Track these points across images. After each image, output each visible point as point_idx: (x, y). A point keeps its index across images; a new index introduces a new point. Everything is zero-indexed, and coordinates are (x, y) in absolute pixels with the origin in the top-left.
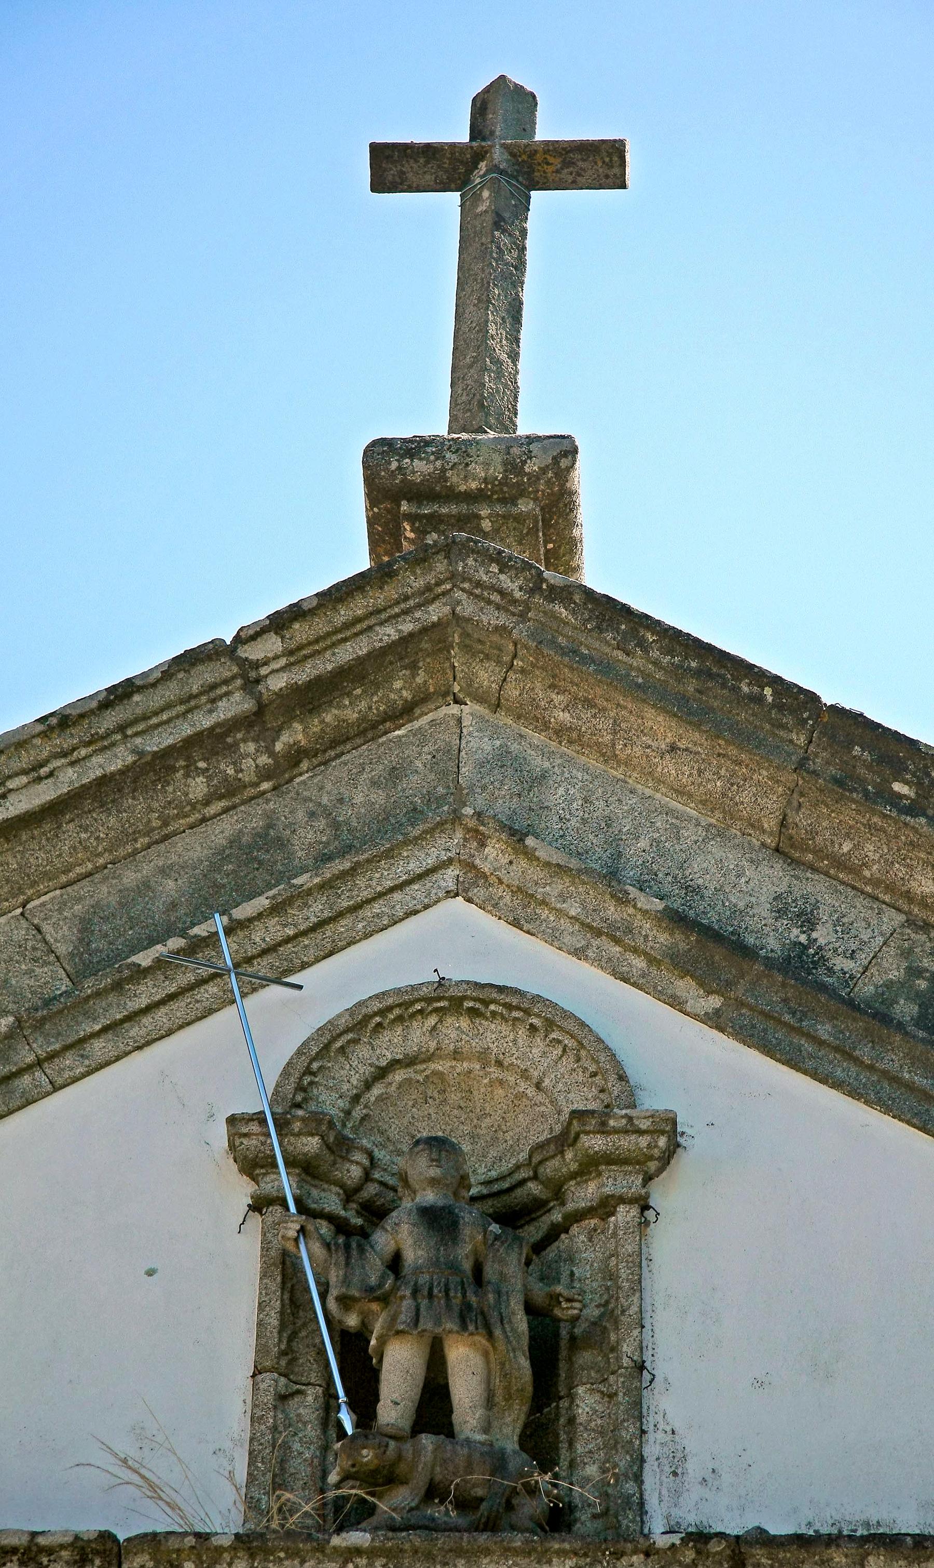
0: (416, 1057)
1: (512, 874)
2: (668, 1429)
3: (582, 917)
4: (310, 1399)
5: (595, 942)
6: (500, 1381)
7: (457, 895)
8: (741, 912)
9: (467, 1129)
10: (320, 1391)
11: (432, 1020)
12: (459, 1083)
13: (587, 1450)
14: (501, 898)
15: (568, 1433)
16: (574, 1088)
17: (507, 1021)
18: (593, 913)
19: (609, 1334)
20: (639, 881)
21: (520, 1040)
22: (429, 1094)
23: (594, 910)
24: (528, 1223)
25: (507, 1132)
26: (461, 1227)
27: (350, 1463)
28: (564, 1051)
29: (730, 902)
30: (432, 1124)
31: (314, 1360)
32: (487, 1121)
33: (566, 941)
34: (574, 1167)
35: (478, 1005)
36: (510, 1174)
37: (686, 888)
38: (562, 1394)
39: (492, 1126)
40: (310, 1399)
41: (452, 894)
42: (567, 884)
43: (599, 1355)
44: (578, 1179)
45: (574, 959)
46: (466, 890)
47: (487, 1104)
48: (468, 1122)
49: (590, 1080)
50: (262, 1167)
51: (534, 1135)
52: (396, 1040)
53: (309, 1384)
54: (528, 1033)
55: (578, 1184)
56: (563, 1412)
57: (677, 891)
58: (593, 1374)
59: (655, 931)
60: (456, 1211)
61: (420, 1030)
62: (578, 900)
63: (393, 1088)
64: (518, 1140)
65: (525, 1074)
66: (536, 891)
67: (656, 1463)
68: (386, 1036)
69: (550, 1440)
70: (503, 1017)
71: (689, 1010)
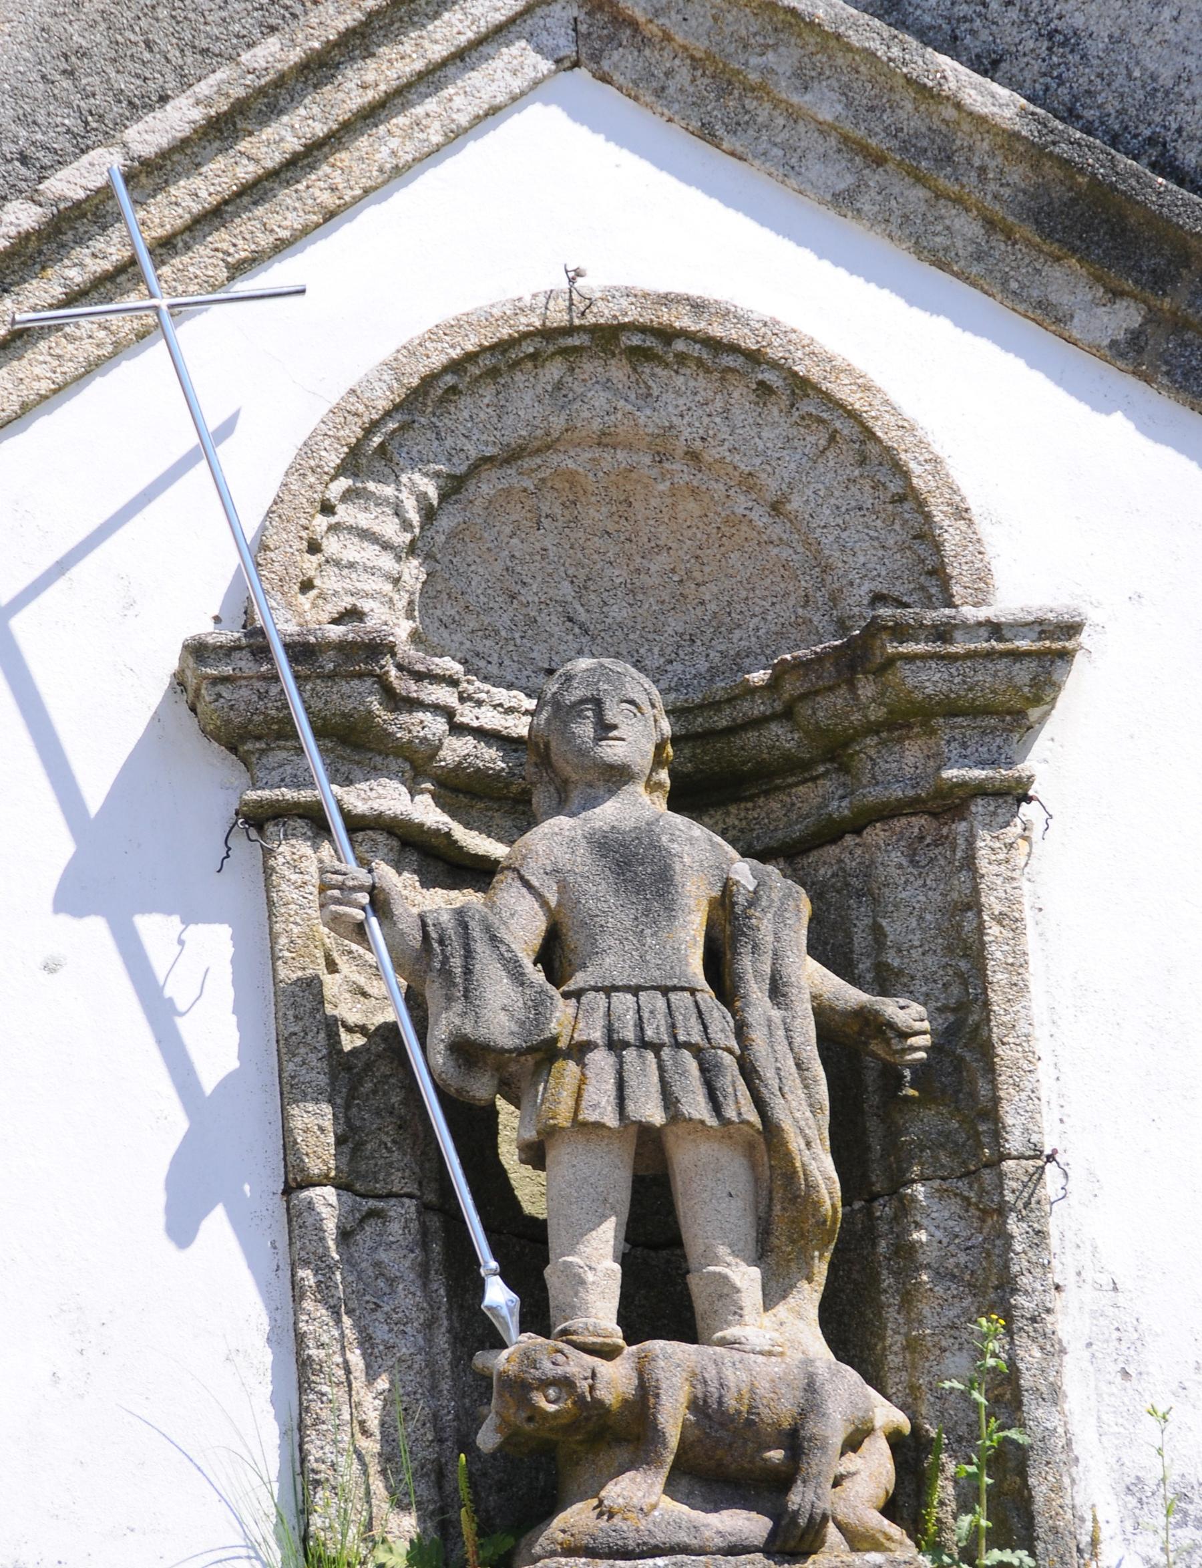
0: (522, 448)
1: (693, 23)
2: (1105, 1280)
3: (848, 127)
4: (395, 1227)
5: (875, 178)
6: (784, 1209)
7: (576, 64)
8: (1167, 93)
9: (619, 574)
10: (413, 1209)
11: (554, 370)
12: (606, 488)
13: (944, 1321)
14: (668, 74)
15: (896, 1274)
16: (855, 519)
17: (708, 371)
18: (870, 115)
19: (973, 1082)
20: (949, 19)
21: (736, 411)
22: (545, 509)
23: (871, 109)
24: (766, 793)
25: (704, 583)
26: (678, 879)
27: (524, 1415)
28: (832, 438)
29: (1144, 69)
30: (550, 569)
31: (394, 1142)
32: (660, 562)
33: (812, 175)
34: (876, 713)
35: (650, 342)
36: (729, 701)
37: (1050, 36)
38: (877, 1188)
39: (673, 571)
40: (395, 1227)
41: (567, 64)
42: (811, 48)
43: (953, 1117)
44: (884, 735)
45: (832, 213)
46: (596, 57)
47: (662, 528)
48: (623, 560)
49: (890, 507)
50: (258, 738)
51: (764, 598)
52: (482, 416)
53: (390, 1195)
54: (753, 397)
55: (883, 743)
56: (883, 1228)
57: (1031, 44)
58: (944, 1159)
59: (1000, 159)
60: (664, 838)
61: (531, 392)
62: (836, 85)
63: (478, 509)
64: (729, 603)
65: (748, 483)
66: (746, 64)
67: (1086, 1354)
68: (465, 407)
69: (855, 1276)
70: (700, 363)
71: (1076, 334)
